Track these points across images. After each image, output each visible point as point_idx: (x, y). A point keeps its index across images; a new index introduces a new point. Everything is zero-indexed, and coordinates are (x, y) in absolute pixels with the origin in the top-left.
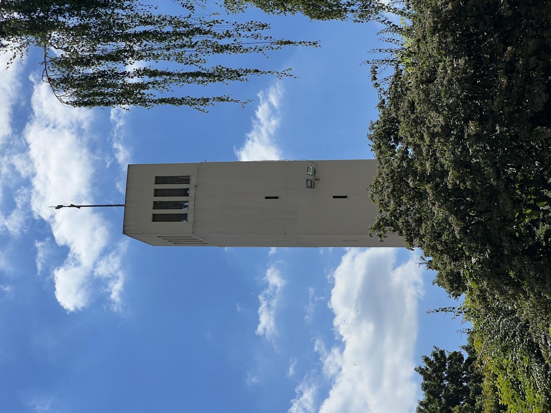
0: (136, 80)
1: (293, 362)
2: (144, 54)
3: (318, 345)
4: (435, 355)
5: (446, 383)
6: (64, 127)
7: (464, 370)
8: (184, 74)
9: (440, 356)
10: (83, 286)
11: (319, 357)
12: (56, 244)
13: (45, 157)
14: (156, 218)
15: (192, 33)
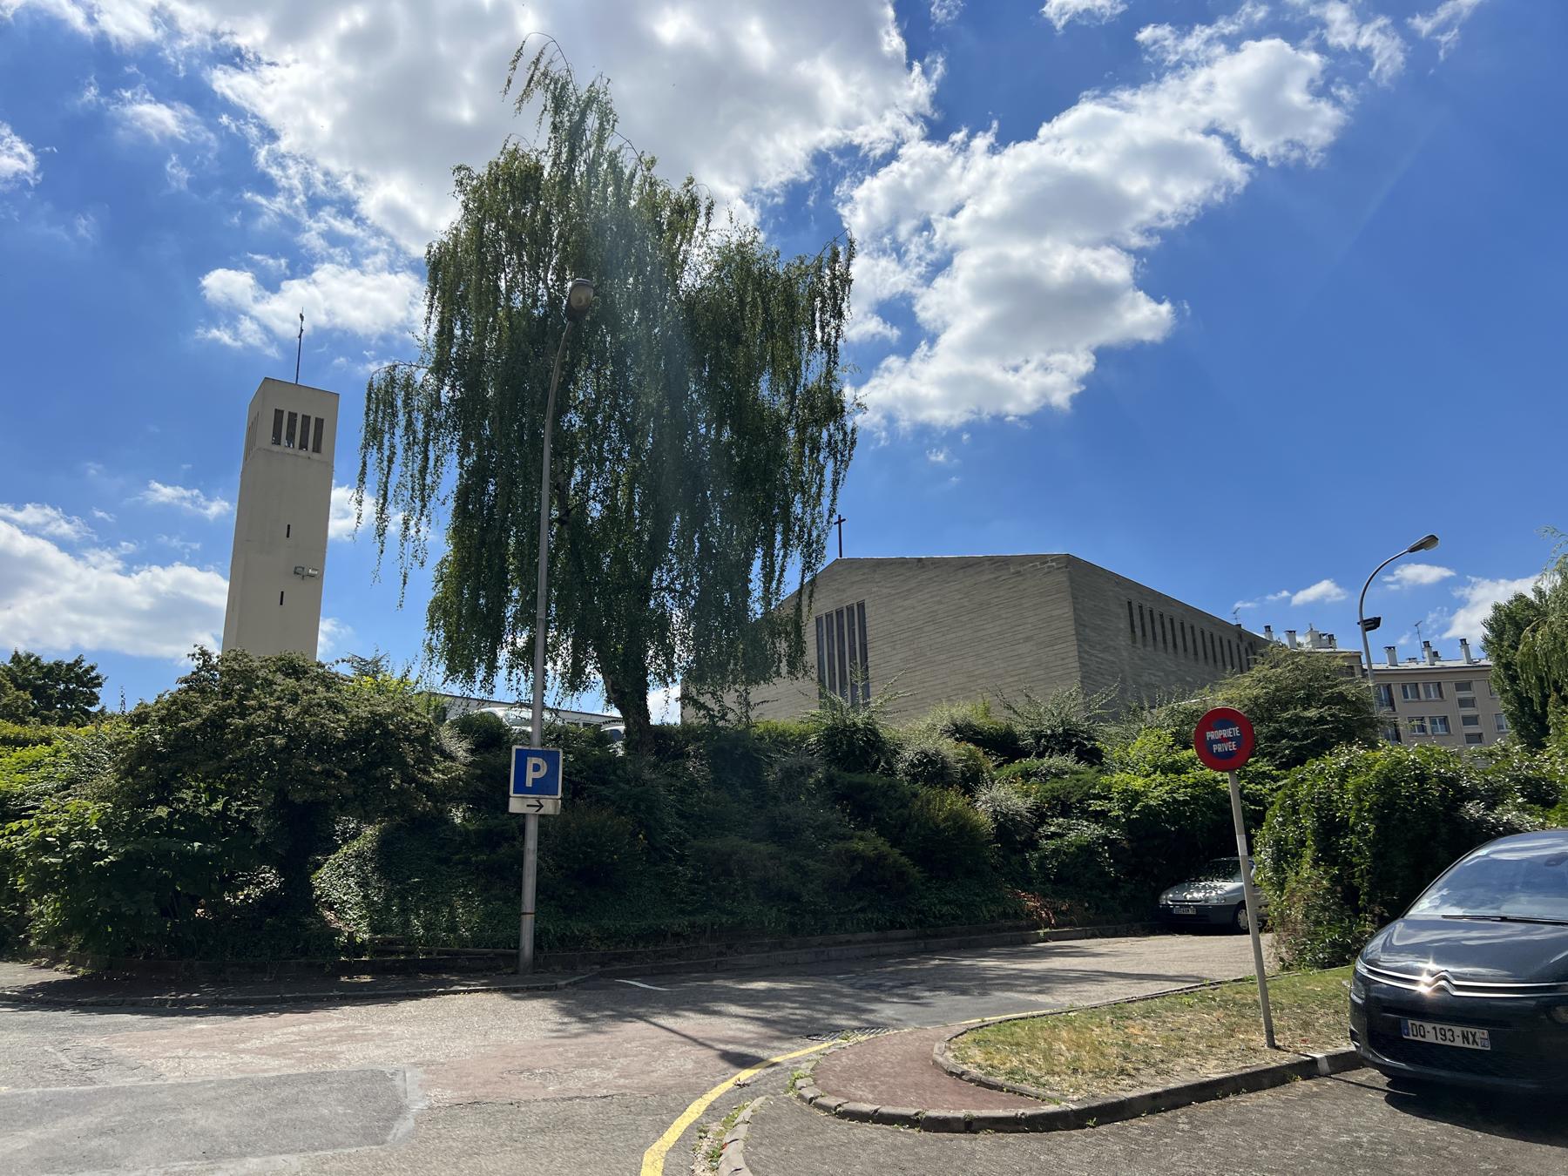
0: (386, 444)
1: (111, 517)
2: (410, 454)
3: (127, 547)
4: (97, 677)
5: (62, 687)
6: (409, 313)
7: (77, 706)
8: (386, 487)
9: (96, 682)
10: (230, 300)
11: (111, 547)
12: (282, 280)
13: (381, 289)
14: (279, 414)
15: (423, 500)
